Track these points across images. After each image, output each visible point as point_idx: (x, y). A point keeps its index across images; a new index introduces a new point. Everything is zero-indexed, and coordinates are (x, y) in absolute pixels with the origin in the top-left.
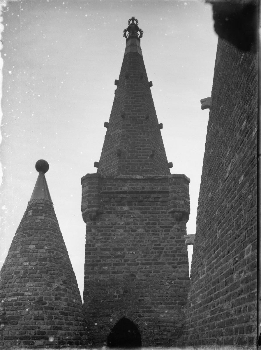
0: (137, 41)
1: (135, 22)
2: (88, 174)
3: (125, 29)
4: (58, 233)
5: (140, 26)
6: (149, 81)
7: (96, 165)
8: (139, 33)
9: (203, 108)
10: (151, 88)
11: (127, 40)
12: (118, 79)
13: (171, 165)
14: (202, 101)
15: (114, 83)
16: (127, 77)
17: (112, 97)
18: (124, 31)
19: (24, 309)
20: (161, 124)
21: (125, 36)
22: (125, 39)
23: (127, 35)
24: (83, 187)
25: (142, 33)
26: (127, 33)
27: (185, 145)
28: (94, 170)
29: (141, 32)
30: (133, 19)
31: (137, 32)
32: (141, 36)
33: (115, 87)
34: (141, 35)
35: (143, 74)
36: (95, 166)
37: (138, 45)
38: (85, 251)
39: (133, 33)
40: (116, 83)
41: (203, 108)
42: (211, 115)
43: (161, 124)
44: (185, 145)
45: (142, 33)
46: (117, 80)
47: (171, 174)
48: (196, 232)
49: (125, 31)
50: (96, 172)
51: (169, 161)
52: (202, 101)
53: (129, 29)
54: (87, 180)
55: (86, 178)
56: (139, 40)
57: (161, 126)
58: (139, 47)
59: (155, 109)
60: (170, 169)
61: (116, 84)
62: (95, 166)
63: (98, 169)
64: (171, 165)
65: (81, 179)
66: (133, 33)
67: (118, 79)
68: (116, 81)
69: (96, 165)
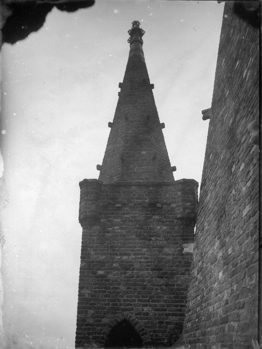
0: (140, 45)
6: (161, 122)
7: (99, 167)
9: (204, 118)
10: (163, 130)
13: (174, 169)
15: (118, 86)
19: (152, 294)
27: (187, 151)
33: (119, 90)
35: (146, 79)
39: (136, 34)
40: (121, 85)
42: (215, 88)
44: (187, 151)
48: (213, 104)
52: (204, 112)
54: (85, 184)
57: (163, 126)
59: (164, 139)
60: (173, 172)
66: (136, 34)
68: (120, 83)
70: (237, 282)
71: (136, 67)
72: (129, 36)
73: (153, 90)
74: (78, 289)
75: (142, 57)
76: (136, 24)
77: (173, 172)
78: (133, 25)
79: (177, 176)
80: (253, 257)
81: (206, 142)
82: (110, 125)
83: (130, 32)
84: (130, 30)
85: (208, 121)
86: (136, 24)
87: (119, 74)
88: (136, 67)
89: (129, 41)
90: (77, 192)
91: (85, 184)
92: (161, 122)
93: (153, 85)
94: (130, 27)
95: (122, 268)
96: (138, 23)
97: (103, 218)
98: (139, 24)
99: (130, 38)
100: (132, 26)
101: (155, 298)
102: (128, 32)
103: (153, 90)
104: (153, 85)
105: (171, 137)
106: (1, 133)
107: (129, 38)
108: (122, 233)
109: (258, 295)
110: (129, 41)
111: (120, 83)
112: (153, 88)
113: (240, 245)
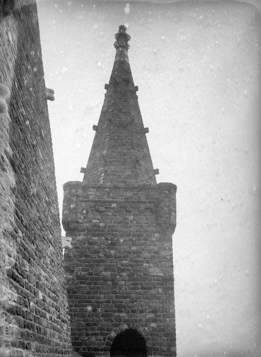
33: (105, 91)
39: (122, 39)
40: (107, 87)
66: (122, 39)
68: (106, 85)
72: (115, 40)
74: (174, 273)
75: (127, 62)
76: (122, 28)
78: (120, 30)
80: (81, 202)
83: (116, 36)
84: (116, 34)
86: (122, 28)
87: (105, 75)
89: (115, 46)
93: (137, 87)
94: (117, 31)
95: (151, 242)
96: (124, 28)
98: (125, 29)
99: (116, 42)
100: (119, 30)
102: (115, 44)
104: (137, 87)
107: (114, 42)
108: (36, 25)
109: (87, 203)
110: (115, 46)
111: (106, 85)
113: (115, 245)
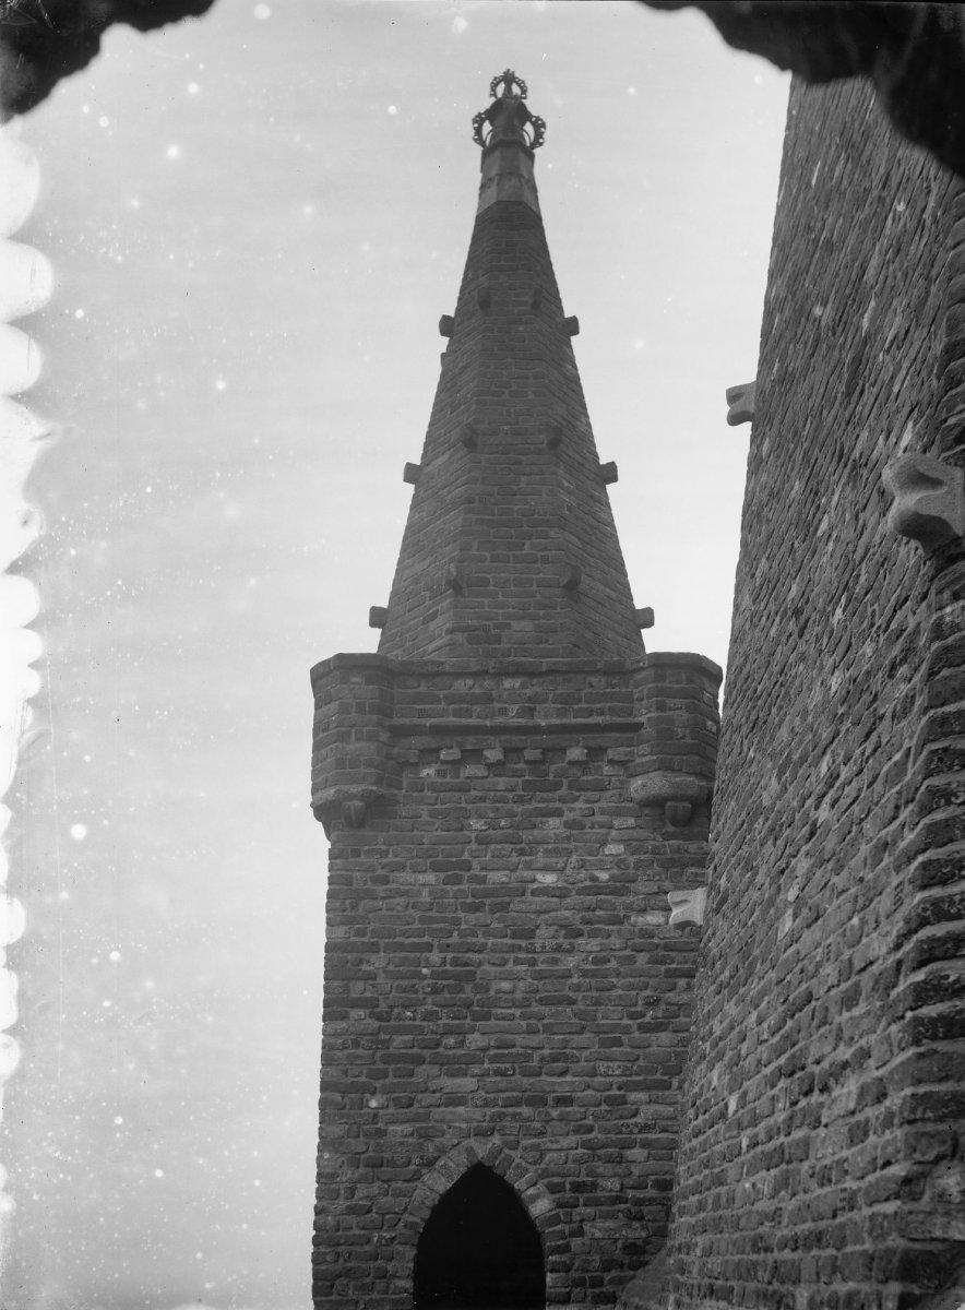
0: (522, 156)
1: (516, 90)
2: (340, 657)
3: (479, 115)
4: (349, 881)
5: (533, 105)
7: (377, 617)
8: (529, 127)
9: (735, 419)
11: (485, 155)
12: (452, 314)
13: (647, 618)
14: (734, 396)
16: (485, 304)
17: (435, 370)
18: (474, 121)
20: (612, 467)
21: (479, 139)
22: (479, 149)
23: (484, 137)
24: (317, 707)
25: (543, 130)
26: (487, 127)
27: (684, 574)
28: (367, 641)
29: (539, 126)
30: (509, 78)
31: (524, 125)
32: (537, 142)
34: (539, 135)
36: (373, 624)
37: (525, 173)
38: (319, 1094)
39: (508, 130)
40: (447, 326)
41: (735, 419)
43: (612, 467)
44: (684, 574)
45: (543, 130)
46: (415, 466)
47: (648, 651)
49: (479, 120)
50: (374, 650)
51: (639, 603)
52: (734, 396)
53: (491, 114)
54: (332, 676)
55: (337, 668)
56: (531, 157)
57: (610, 473)
58: (528, 181)
60: (644, 632)
61: (444, 332)
62: (373, 624)
63: (383, 634)
64: (647, 618)
65: (313, 671)
66: (508, 130)
67: (452, 314)
69: (377, 617)
70: (782, 1000)
71: (509, 244)
73: (573, 338)
77: (644, 632)
79: (655, 641)
81: (738, 559)
82: (412, 473)
85: (748, 425)
87: (438, 276)
88: (509, 244)
90: (302, 707)
91: (332, 676)
92: (603, 461)
97: (539, 1032)
101: (486, 601)
103: (573, 338)
105: (630, 509)
106: (431, 1217)
112: (576, 331)
